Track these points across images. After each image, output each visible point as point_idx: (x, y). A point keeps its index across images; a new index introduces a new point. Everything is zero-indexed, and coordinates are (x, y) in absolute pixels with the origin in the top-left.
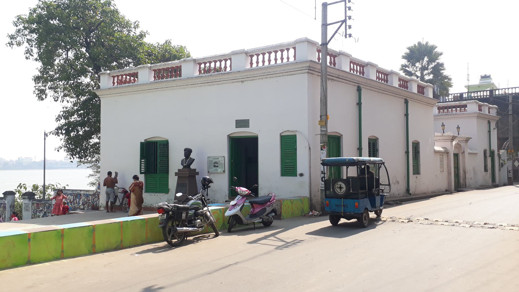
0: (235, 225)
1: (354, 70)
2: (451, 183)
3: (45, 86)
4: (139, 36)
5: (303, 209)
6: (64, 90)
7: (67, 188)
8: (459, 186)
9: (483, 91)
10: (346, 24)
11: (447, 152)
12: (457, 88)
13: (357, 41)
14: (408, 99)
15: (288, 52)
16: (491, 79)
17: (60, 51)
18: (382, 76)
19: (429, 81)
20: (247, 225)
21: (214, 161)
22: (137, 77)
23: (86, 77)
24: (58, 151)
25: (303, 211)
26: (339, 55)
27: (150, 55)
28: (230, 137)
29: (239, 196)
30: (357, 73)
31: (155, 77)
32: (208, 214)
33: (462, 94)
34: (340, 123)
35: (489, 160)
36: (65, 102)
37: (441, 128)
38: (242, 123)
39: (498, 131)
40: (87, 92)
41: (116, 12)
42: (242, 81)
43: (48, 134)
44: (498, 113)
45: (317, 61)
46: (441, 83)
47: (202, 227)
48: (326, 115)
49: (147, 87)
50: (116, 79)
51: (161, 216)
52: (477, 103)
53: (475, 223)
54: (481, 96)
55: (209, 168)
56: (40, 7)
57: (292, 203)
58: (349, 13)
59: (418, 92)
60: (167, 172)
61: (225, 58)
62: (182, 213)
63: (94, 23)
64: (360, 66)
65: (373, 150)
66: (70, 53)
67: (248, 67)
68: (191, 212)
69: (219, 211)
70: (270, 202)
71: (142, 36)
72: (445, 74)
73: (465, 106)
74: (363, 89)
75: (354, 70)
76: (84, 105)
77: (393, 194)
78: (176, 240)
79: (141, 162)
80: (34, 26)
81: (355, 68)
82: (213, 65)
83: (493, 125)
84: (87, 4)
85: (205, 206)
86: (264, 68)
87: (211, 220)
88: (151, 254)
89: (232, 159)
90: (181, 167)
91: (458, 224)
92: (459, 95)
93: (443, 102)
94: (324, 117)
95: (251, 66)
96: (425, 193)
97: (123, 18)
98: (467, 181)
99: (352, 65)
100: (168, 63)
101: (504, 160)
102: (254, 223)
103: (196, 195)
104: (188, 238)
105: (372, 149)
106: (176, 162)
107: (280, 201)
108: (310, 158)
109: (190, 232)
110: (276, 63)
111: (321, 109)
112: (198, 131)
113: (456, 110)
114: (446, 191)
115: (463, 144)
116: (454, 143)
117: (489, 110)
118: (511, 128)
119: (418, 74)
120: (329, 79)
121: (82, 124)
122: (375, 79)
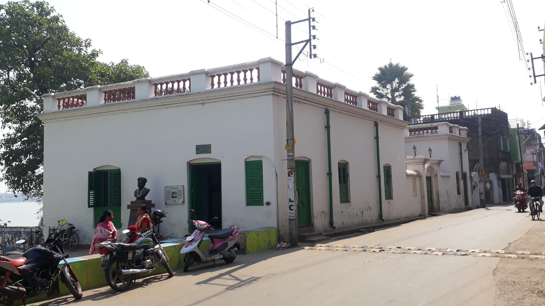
0: (192, 263)
1: (321, 92)
2: (425, 207)
4: (91, 55)
5: (270, 241)
8: (433, 210)
10: (310, 43)
11: (419, 176)
12: (429, 109)
13: (322, 61)
14: (377, 121)
15: (251, 72)
16: (461, 100)
19: (400, 103)
20: (207, 262)
21: (173, 191)
22: (85, 100)
25: (270, 243)
26: (305, 76)
27: (103, 75)
28: (190, 164)
29: (196, 231)
30: (324, 95)
31: (105, 99)
32: (161, 252)
33: (433, 116)
34: (308, 147)
35: (462, 182)
36: (7, 128)
37: (412, 151)
38: (203, 149)
39: (469, 152)
40: (32, 117)
41: (65, 29)
45: (282, 82)
46: (412, 104)
47: (152, 268)
48: (293, 139)
49: (97, 110)
50: (62, 102)
51: (104, 257)
52: (447, 125)
53: (448, 250)
55: (166, 198)
57: (258, 235)
59: (388, 114)
60: (119, 204)
61: (183, 78)
63: (40, 41)
64: (328, 87)
66: (11, 74)
67: (209, 88)
69: (173, 249)
70: (232, 235)
71: (94, 55)
73: (436, 128)
74: (331, 112)
76: (27, 132)
77: (366, 220)
78: (122, 284)
79: (89, 194)
81: (323, 90)
82: (164, 86)
83: (464, 147)
84: (31, 19)
85: (157, 244)
86: (226, 89)
87: (163, 259)
88: (89, 302)
90: (134, 199)
91: (430, 252)
92: (430, 116)
93: (414, 124)
95: (213, 87)
96: (398, 219)
97: (73, 35)
100: (122, 83)
101: (476, 183)
102: (214, 260)
104: (137, 281)
105: (342, 173)
107: (244, 235)
108: (278, 186)
109: (139, 273)
111: (287, 133)
112: (154, 156)
114: (420, 215)
115: (435, 167)
116: (426, 166)
117: (460, 132)
119: (389, 96)
120: (295, 101)
121: (25, 152)
122: (343, 101)
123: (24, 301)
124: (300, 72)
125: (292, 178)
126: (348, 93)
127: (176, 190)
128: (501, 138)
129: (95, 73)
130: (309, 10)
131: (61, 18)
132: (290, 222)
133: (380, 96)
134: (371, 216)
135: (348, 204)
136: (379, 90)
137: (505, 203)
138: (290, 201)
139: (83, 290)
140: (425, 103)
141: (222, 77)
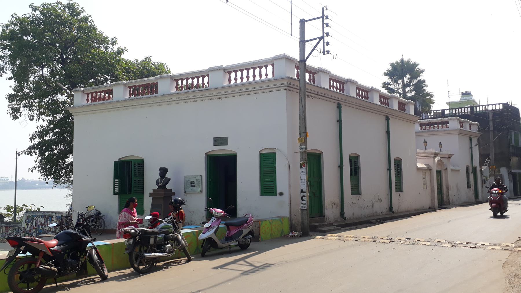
1: (333, 87)
2: (434, 200)
3: (19, 105)
4: (117, 52)
6: (39, 108)
7: (41, 210)
8: (443, 203)
9: (465, 108)
10: (324, 40)
11: (429, 169)
12: (439, 104)
13: (335, 57)
14: (389, 115)
15: (266, 68)
16: (472, 95)
17: (35, 67)
18: (362, 93)
19: (411, 98)
20: (222, 248)
21: (192, 180)
22: (112, 94)
23: (63, 94)
24: (32, 171)
27: (127, 71)
28: (208, 155)
29: (213, 218)
30: (337, 90)
31: (130, 94)
33: (443, 111)
34: (321, 140)
35: (472, 176)
36: (41, 121)
37: (423, 145)
38: (220, 141)
41: (93, 28)
42: (220, 98)
43: (20, 153)
44: (479, 130)
45: (296, 78)
46: (423, 100)
47: (172, 252)
48: (306, 132)
49: (122, 104)
50: (90, 96)
51: (128, 241)
52: (458, 119)
53: (457, 243)
54: (462, 113)
56: (12, 23)
57: (271, 224)
58: (327, 30)
60: (142, 192)
61: (202, 74)
62: (149, 238)
63: (71, 40)
65: (355, 167)
66: (45, 70)
67: (226, 83)
68: (160, 237)
69: (192, 235)
70: (247, 223)
71: (120, 52)
72: (426, 91)
73: (447, 123)
74: (343, 106)
75: (333, 87)
78: (144, 266)
79: (114, 182)
80: (6, 42)
81: (335, 85)
83: (475, 141)
84: (63, 20)
86: (242, 85)
87: (182, 245)
88: (114, 282)
89: (210, 178)
90: (156, 187)
91: (440, 244)
92: (440, 111)
93: (425, 119)
94: (303, 135)
95: (230, 83)
96: (408, 211)
97: (101, 34)
98: (450, 198)
99: (332, 82)
100: (145, 79)
101: (486, 177)
102: (230, 247)
103: (167, 217)
104: (158, 264)
105: (353, 166)
106: (151, 181)
107: (258, 223)
108: (290, 178)
109: (159, 257)
110: (254, 79)
111: (300, 126)
112: (175, 149)
113: (438, 127)
114: (430, 208)
115: (445, 161)
116: (437, 160)
117: (470, 127)
118: (492, 144)
119: (401, 91)
121: (57, 143)
123: (55, 279)
124: (313, 68)
125: (304, 170)
126: (359, 88)
127: (194, 180)
128: (513, 133)
129: (120, 69)
130: (323, 8)
131: (90, 18)
132: (302, 212)
133: (392, 91)
134: (382, 208)
135: (359, 195)
136: (391, 85)
137: (516, 197)
138: (302, 192)
139: (109, 271)
140: (435, 99)
141: (239, 74)
